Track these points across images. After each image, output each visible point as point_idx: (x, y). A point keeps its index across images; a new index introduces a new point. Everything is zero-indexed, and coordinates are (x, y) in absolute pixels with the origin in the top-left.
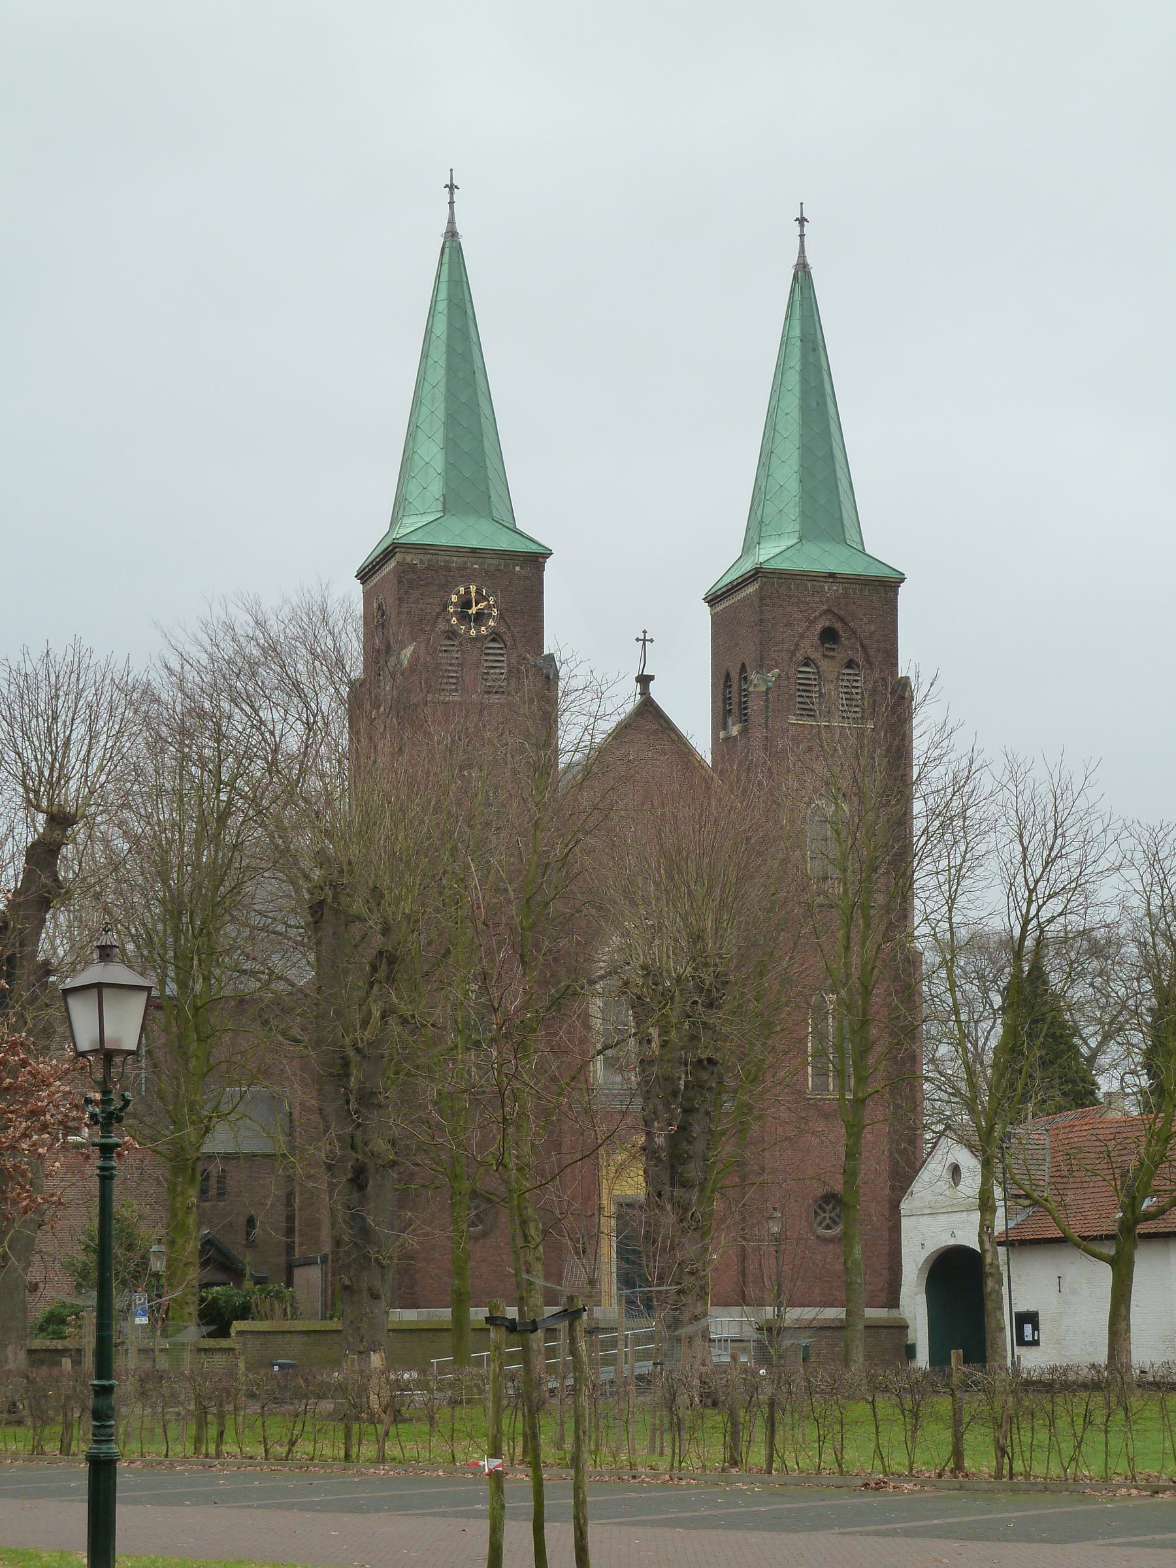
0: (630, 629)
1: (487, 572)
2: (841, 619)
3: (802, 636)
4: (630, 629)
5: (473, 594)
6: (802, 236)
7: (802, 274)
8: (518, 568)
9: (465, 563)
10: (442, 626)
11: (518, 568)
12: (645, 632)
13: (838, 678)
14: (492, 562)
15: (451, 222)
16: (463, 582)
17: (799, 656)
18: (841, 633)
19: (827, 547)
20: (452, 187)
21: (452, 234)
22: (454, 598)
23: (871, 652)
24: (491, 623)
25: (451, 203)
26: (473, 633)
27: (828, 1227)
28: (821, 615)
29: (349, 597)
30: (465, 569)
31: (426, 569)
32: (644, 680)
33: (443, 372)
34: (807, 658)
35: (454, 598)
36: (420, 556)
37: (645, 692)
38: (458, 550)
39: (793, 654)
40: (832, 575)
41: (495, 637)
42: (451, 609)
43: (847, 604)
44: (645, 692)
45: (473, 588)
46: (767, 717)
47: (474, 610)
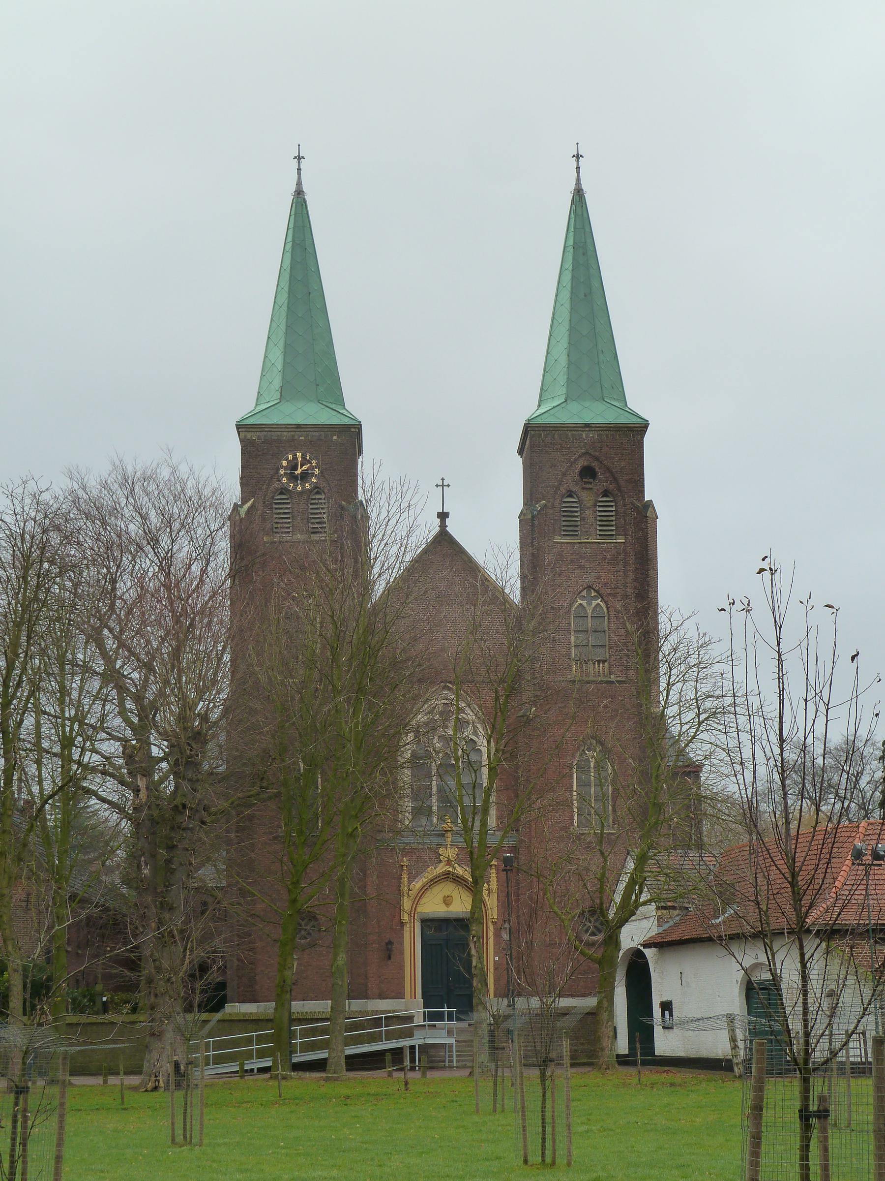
0: (445, 479)
1: (310, 442)
2: (597, 459)
3: (564, 474)
4: (445, 479)
5: (300, 459)
6: (578, 168)
7: (579, 195)
8: (335, 438)
9: (293, 436)
10: (276, 485)
11: (335, 438)
12: (443, 479)
13: (595, 506)
14: (314, 434)
15: (299, 183)
16: (291, 451)
17: (563, 490)
18: (597, 469)
19: (587, 404)
20: (578, 157)
21: (299, 193)
22: (284, 463)
23: (622, 482)
24: (314, 480)
25: (578, 168)
26: (299, 488)
27: (593, 934)
28: (580, 457)
29: (220, 471)
30: (293, 440)
31: (263, 442)
32: (443, 516)
33: (286, 295)
34: (571, 491)
35: (284, 463)
36: (258, 433)
37: (443, 526)
38: (286, 427)
39: (558, 488)
40: (587, 425)
41: (317, 489)
42: (282, 472)
43: (601, 448)
44: (443, 526)
45: (299, 455)
46: (533, 539)
47: (299, 471)
